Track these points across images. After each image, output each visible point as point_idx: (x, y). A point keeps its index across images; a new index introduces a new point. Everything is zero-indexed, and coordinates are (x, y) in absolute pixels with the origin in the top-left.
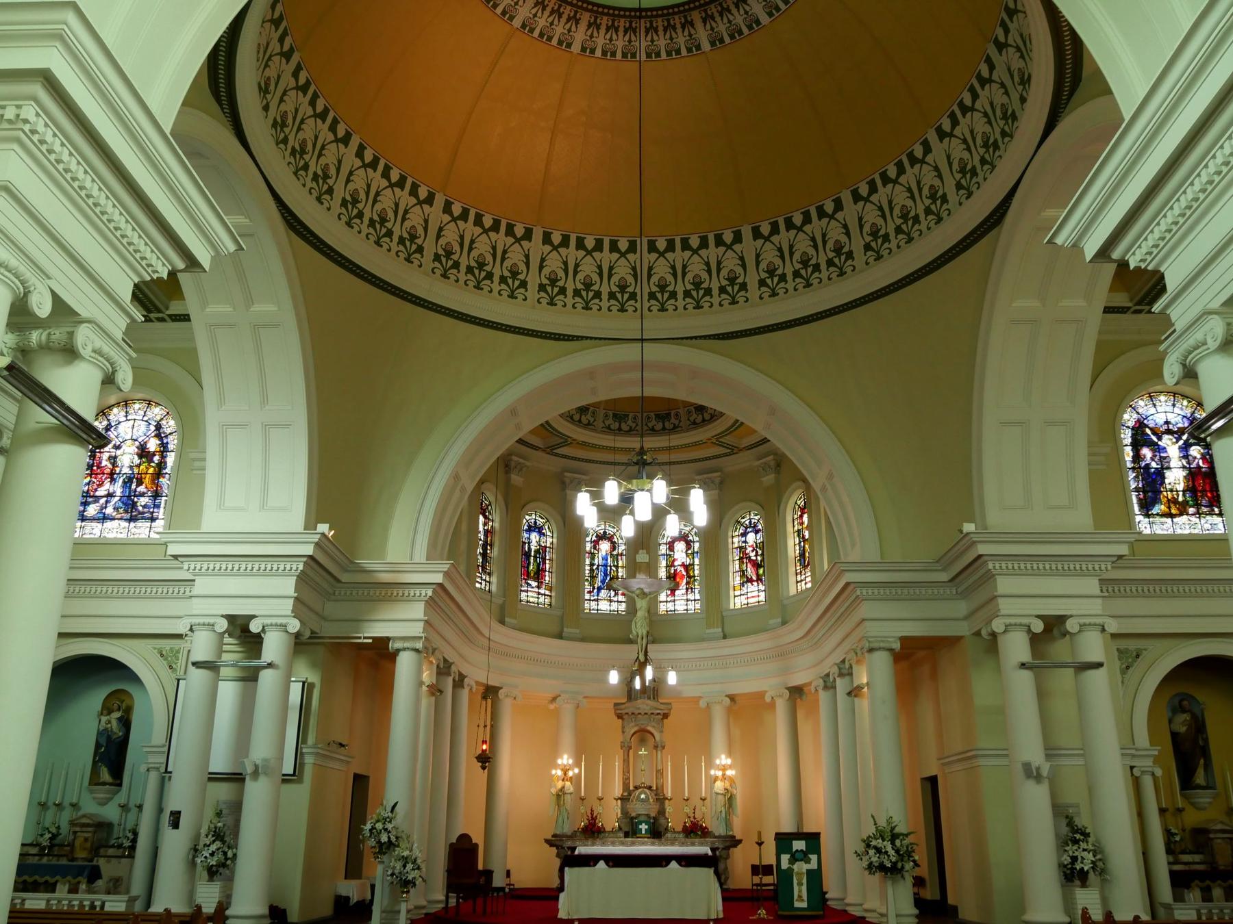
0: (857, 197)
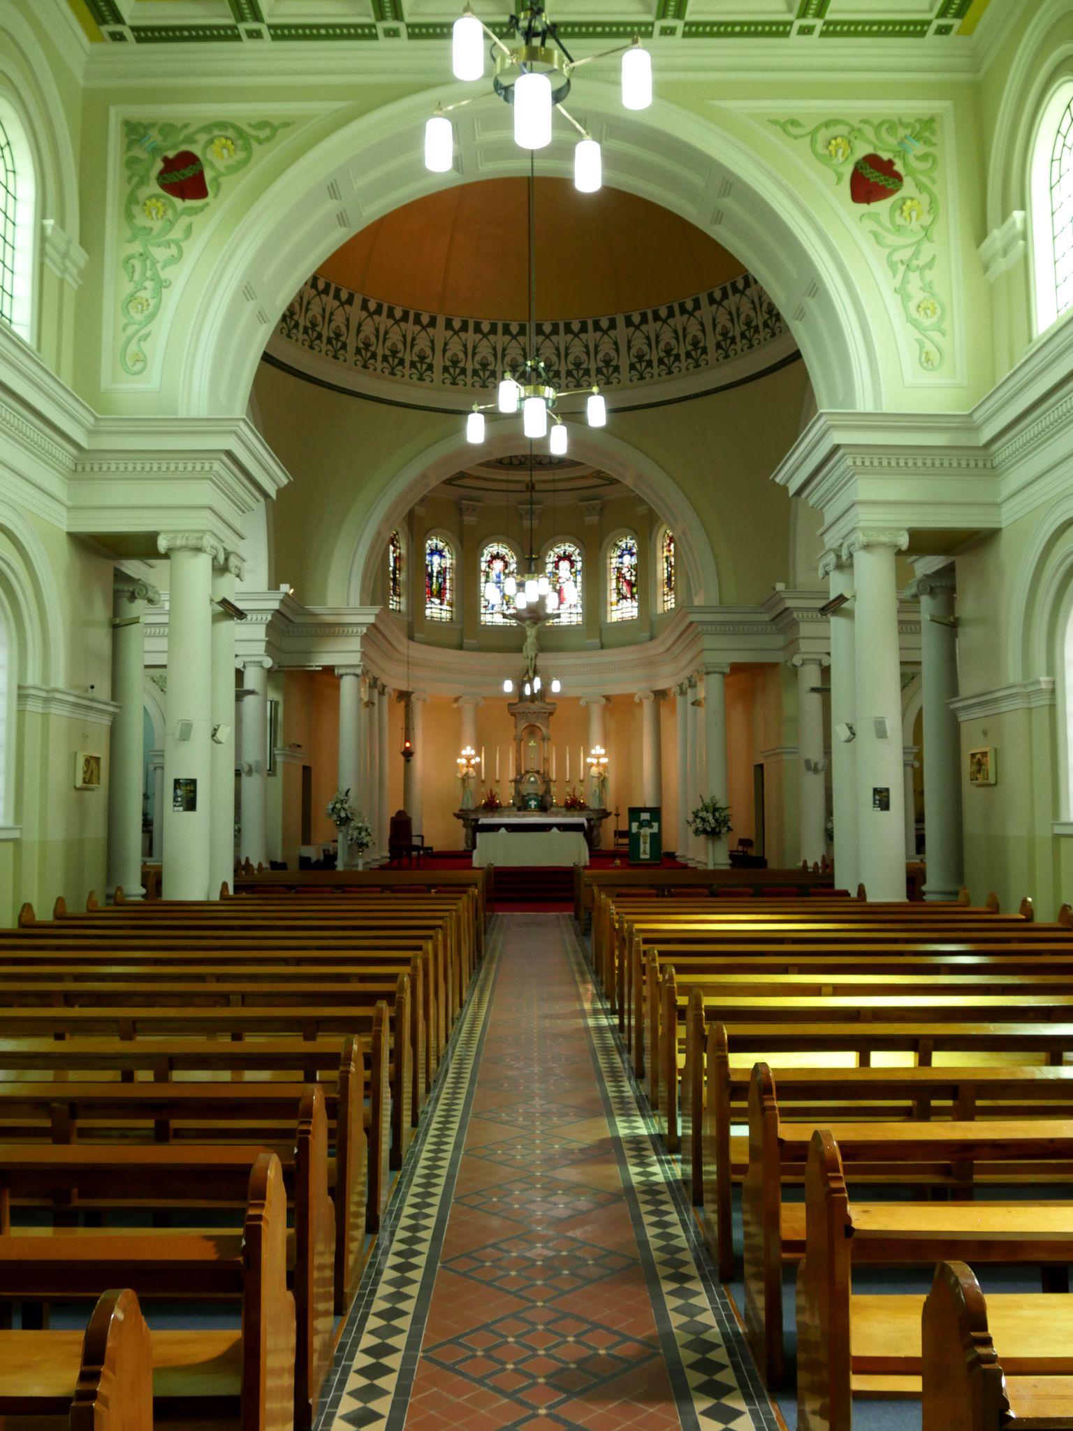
0: (712, 300)
